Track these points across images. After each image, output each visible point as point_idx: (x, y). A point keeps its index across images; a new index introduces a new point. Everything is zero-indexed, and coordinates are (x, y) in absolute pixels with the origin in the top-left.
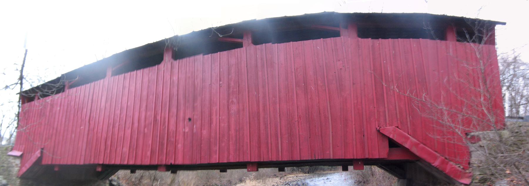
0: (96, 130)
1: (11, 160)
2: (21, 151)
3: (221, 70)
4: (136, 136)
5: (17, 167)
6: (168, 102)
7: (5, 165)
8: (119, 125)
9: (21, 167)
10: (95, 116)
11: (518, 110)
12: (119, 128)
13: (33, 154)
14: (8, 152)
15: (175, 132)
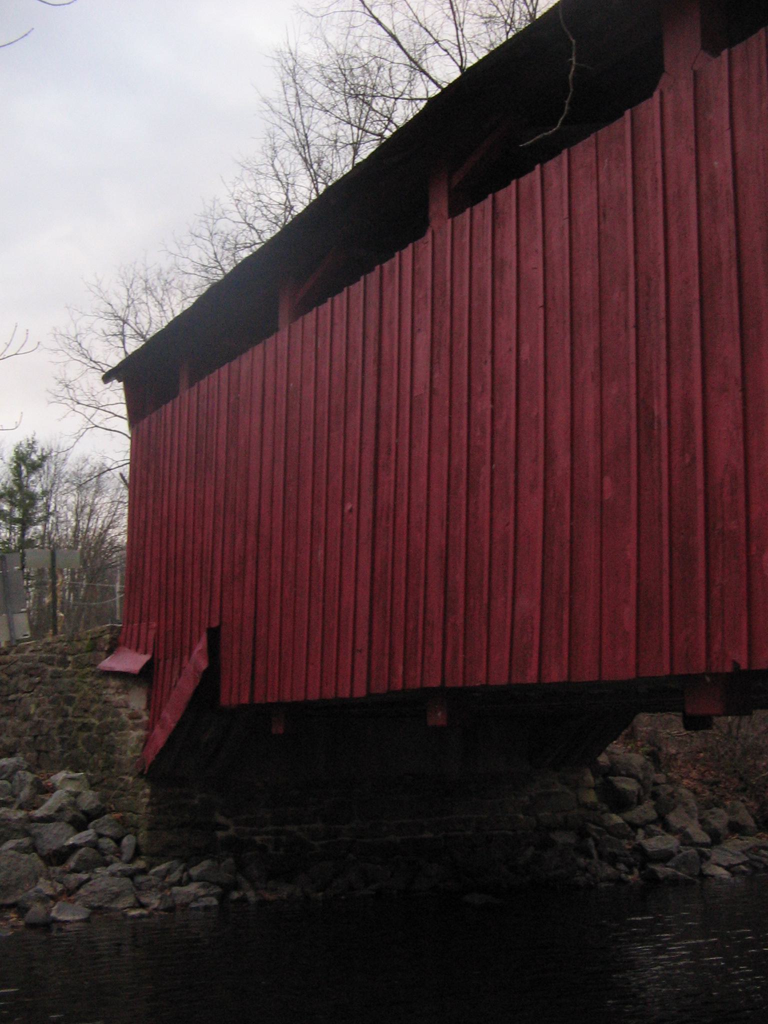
0: (403, 511)
1: (112, 693)
2: (145, 653)
3: (291, 385)
4: (567, 528)
5: (135, 727)
6: (697, 306)
7: (95, 721)
8: (492, 473)
9: (149, 727)
10: (393, 441)
11: (143, 857)
12: (492, 488)
13: (186, 657)
14: (101, 660)
15: (741, 480)
